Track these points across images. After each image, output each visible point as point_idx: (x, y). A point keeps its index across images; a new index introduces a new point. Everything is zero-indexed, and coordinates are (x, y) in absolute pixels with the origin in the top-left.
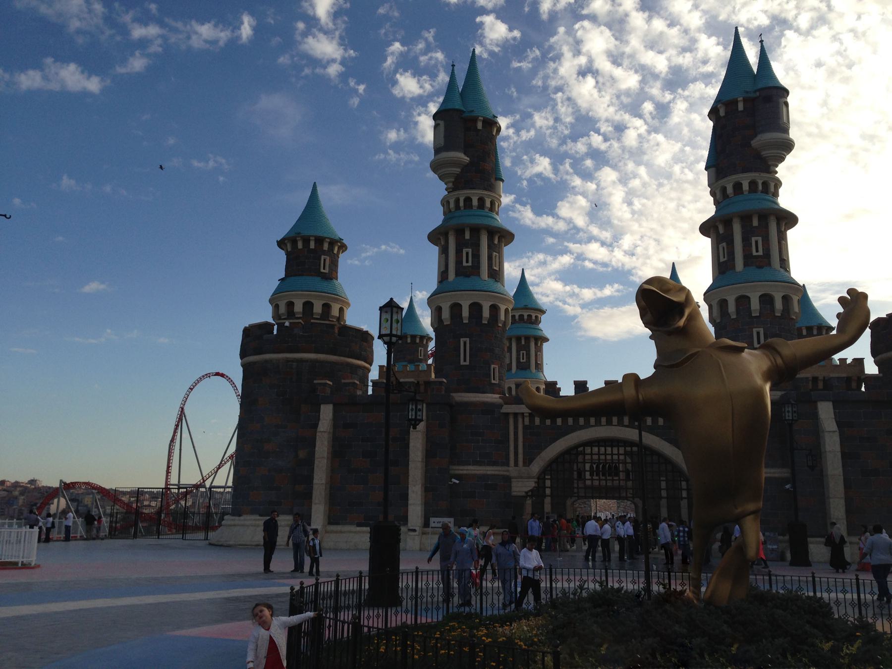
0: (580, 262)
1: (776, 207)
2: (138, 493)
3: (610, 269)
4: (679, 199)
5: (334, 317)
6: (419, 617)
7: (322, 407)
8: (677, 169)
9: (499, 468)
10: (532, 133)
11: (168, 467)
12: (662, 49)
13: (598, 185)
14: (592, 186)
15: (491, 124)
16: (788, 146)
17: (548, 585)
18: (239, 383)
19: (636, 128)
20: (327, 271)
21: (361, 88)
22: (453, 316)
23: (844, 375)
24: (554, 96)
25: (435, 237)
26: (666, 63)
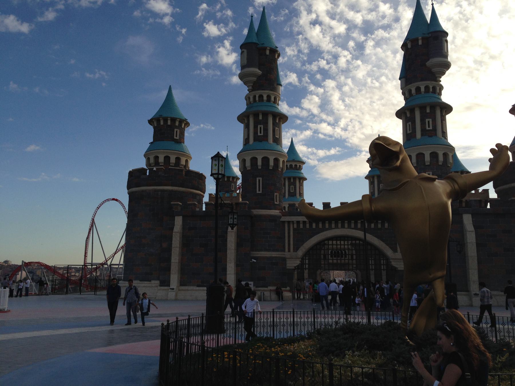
0: (316, 135)
1: (440, 101)
2: (68, 268)
3: (333, 139)
4: (371, 98)
5: (183, 165)
6: (237, 340)
7: (176, 218)
8: (369, 80)
9: (280, 253)
10: (286, 59)
11: (86, 253)
12: (358, 9)
13: (324, 90)
14: (321, 90)
15: (275, 53)
16: (447, 66)
17: (313, 320)
18: (126, 203)
19: (345, 56)
20: (178, 138)
21: (184, 31)
22: (252, 165)
23: (479, 199)
24: (297, 37)
25: (242, 118)
26: (361, 18)
